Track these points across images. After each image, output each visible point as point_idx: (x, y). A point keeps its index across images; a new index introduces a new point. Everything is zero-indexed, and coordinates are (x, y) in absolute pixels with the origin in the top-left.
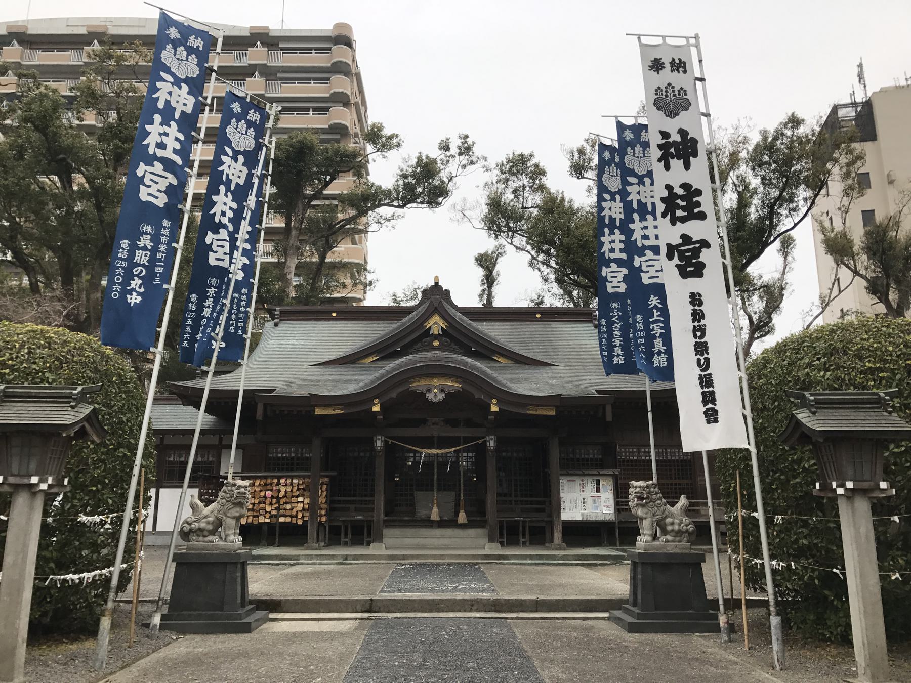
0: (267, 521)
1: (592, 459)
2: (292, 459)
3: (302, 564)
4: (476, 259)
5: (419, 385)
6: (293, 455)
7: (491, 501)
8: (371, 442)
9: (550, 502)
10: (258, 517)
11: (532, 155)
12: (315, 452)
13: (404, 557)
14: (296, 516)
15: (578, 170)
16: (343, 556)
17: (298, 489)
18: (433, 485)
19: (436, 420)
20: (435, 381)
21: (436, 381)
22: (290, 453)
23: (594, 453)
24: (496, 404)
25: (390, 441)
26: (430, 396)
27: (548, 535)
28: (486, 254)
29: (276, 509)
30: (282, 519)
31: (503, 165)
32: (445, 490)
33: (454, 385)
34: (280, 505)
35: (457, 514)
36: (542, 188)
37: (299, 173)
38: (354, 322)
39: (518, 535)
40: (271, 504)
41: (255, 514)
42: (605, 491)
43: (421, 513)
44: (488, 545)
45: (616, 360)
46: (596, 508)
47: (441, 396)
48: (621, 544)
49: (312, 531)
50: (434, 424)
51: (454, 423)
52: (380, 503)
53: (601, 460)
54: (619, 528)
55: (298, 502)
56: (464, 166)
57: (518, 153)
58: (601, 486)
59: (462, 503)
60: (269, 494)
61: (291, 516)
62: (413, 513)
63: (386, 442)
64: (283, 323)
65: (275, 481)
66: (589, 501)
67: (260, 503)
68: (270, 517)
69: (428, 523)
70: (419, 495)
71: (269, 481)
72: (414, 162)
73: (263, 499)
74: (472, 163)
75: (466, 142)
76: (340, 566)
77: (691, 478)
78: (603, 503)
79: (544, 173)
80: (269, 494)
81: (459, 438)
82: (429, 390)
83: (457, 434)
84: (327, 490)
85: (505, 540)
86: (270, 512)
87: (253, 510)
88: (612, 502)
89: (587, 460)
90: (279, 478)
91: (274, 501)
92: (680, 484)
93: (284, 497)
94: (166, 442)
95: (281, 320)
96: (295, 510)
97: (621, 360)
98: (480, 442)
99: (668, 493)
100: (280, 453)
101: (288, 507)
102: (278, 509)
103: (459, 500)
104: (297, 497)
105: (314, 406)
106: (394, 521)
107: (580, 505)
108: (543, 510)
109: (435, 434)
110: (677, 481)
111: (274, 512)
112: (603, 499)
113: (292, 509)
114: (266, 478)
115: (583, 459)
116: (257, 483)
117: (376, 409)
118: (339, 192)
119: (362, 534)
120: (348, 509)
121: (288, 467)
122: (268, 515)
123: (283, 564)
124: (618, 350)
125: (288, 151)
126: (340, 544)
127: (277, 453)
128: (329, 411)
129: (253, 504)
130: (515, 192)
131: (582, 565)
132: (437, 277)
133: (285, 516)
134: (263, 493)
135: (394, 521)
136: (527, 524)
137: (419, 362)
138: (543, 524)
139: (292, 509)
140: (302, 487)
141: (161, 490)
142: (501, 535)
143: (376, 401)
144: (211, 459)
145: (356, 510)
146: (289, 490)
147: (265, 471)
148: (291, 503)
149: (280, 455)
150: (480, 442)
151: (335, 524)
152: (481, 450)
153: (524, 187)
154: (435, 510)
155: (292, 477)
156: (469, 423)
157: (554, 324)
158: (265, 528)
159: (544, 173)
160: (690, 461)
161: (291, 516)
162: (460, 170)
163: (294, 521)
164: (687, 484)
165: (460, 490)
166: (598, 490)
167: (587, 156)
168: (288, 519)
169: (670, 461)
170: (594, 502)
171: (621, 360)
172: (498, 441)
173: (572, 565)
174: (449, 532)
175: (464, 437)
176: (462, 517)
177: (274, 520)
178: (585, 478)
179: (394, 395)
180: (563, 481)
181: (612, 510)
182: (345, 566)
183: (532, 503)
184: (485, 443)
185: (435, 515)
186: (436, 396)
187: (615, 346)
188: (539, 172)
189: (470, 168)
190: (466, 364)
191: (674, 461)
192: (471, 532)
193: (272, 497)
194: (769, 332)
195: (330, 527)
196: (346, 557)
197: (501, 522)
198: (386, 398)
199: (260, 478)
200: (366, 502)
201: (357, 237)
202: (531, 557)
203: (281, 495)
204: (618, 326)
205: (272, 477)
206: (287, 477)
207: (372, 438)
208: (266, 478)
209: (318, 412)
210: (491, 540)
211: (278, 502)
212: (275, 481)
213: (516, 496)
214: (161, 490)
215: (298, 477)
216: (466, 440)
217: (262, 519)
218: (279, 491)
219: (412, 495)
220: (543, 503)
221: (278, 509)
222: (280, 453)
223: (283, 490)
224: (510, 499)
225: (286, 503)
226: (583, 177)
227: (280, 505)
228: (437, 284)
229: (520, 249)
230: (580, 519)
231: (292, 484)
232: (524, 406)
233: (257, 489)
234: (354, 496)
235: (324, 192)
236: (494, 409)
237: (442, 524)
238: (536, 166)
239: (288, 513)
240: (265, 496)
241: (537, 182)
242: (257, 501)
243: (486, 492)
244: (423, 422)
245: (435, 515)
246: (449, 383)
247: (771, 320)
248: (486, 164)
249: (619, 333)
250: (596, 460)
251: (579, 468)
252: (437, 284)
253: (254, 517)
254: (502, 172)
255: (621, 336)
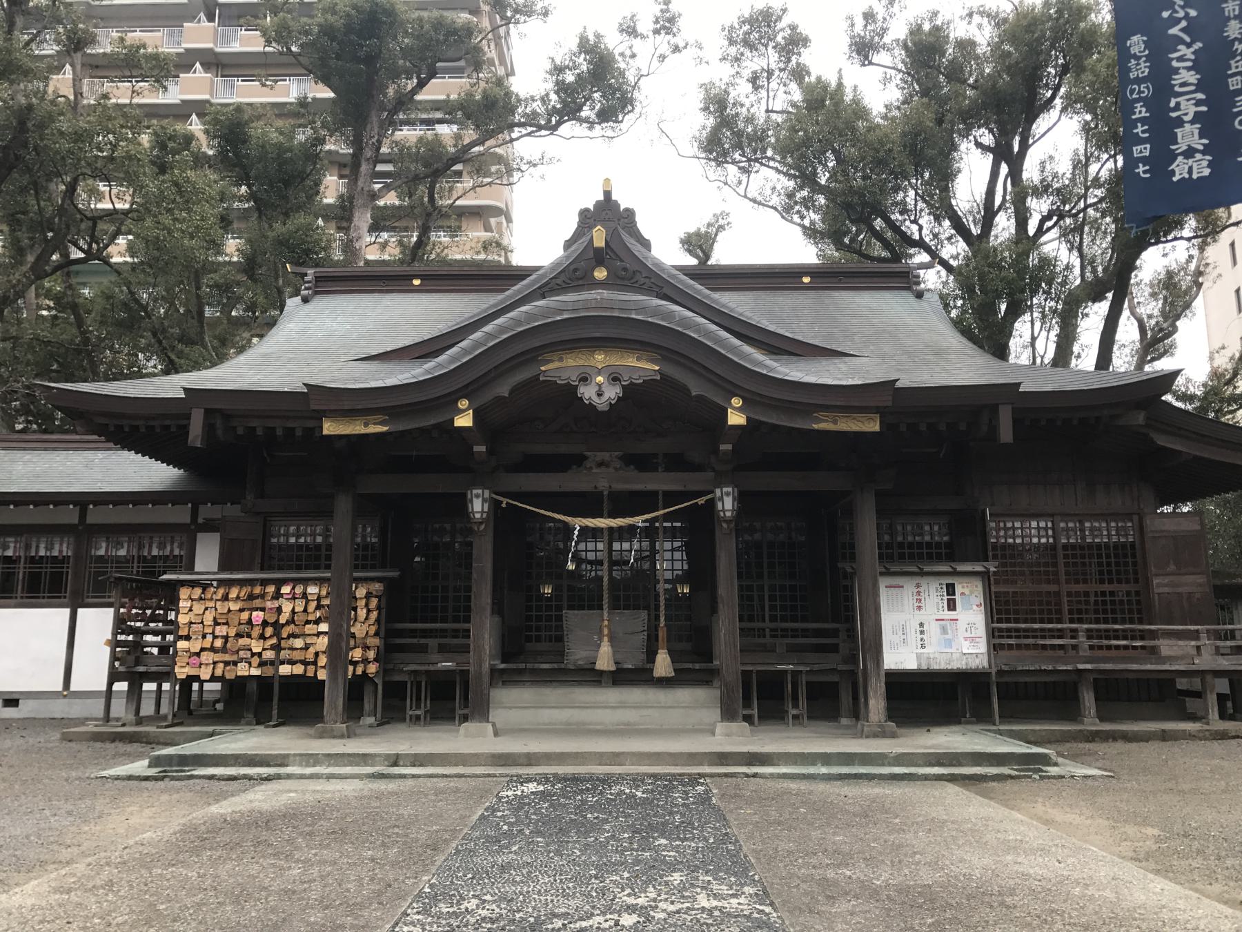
0: (255, 672)
1: (929, 545)
2: (318, 547)
3: (289, 777)
4: (683, 242)
5: (561, 368)
6: (319, 539)
7: (726, 630)
8: (461, 503)
9: (852, 632)
10: (235, 663)
11: (784, 11)
12: (343, 529)
13: (530, 759)
14: (315, 663)
15: (863, 49)
16: (387, 757)
17: (318, 607)
18: (601, 598)
19: (606, 456)
20: (600, 357)
21: (600, 359)
22: (314, 535)
23: (934, 532)
24: (740, 409)
25: (505, 501)
26: (587, 393)
27: (845, 699)
28: (698, 234)
29: (272, 648)
30: (285, 670)
31: (732, 27)
32: (627, 607)
33: (641, 366)
34: (280, 639)
35: (651, 656)
36: (799, 74)
37: (370, 60)
38: (453, 295)
39: (782, 698)
40: (262, 637)
41: (227, 657)
42: (967, 607)
43: (577, 654)
44: (721, 727)
45: (1180, 169)
46: (949, 643)
47: (612, 393)
48: (1007, 716)
49: (334, 699)
50: (601, 464)
51: (642, 463)
52: (485, 634)
53: (948, 545)
54: (998, 684)
55: (319, 634)
56: (663, 58)
57: (760, 6)
58: (957, 597)
59: (662, 634)
60: (258, 616)
61: (305, 663)
62: (561, 654)
63: (495, 505)
64: (318, 297)
65: (271, 589)
66: (933, 629)
67: (239, 635)
68: (262, 664)
69: (590, 676)
70: (572, 618)
71: (257, 590)
72: (573, 44)
73: (245, 628)
74: (676, 49)
75: (667, 11)
76: (381, 785)
77: (1136, 581)
78: (962, 633)
79: (805, 41)
80: (258, 616)
81: (654, 494)
82: (584, 379)
83: (651, 487)
84: (378, 608)
85: (755, 712)
86: (260, 654)
87: (224, 649)
88: (980, 630)
89: (920, 545)
90: (280, 583)
91: (269, 631)
92: (1112, 593)
93: (288, 623)
94: (90, 520)
95: (316, 293)
96: (312, 650)
97: (1201, 168)
98: (701, 501)
99: (1080, 612)
100: (291, 534)
101: (299, 643)
102: (277, 648)
103: (657, 628)
104: (317, 622)
105: (319, 416)
106: (520, 672)
107: (913, 637)
108: (834, 649)
109: (603, 485)
110: (1107, 587)
111: (269, 655)
112: (962, 625)
113: (307, 647)
114: (251, 582)
115: (911, 545)
116: (234, 593)
117: (464, 421)
118: (443, 97)
119: (450, 700)
120: (423, 649)
121: (309, 560)
122: (255, 661)
123: (245, 777)
124: (1189, 136)
125: (348, 15)
126: (404, 720)
127: (287, 535)
128: (356, 428)
129: (226, 638)
130: (754, 80)
131: (952, 779)
132: (607, 180)
133: (292, 662)
134: (245, 616)
135: (520, 672)
136: (804, 679)
137: (561, 311)
138: (835, 678)
139: (307, 647)
140: (326, 602)
141: (80, 611)
142: (747, 703)
143: (463, 404)
144: (176, 552)
145: (443, 649)
146: (299, 609)
147: (262, 569)
148: (304, 635)
149: (292, 540)
150: (701, 501)
151: (397, 678)
152: (698, 528)
153: (770, 73)
154: (606, 648)
155: (306, 582)
156: (677, 463)
157: (837, 295)
158: (253, 687)
159: (805, 41)
160: (1133, 545)
161: (305, 663)
162: (655, 62)
163: (310, 674)
164: (1128, 594)
165: (657, 607)
166: (952, 606)
167: (879, 24)
168: (299, 669)
169: (1090, 546)
170: (944, 630)
171: (1201, 168)
172: (743, 498)
173: (926, 778)
174: (635, 694)
175: (666, 493)
176: (663, 664)
177: (269, 671)
178: (924, 581)
179: (503, 389)
180: (883, 582)
181: (982, 647)
182: (392, 786)
183: (805, 633)
184: (711, 504)
185: (605, 660)
186: (600, 391)
187: (1180, 122)
188: (797, 41)
189: (673, 59)
190: (669, 315)
191: (1099, 546)
192: (684, 695)
193: (265, 623)
194: (1165, 352)
195: (385, 684)
196: (395, 761)
197: (746, 675)
198: (487, 396)
199: (241, 583)
200: (455, 633)
201: (493, 221)
202: (826, 759)
203: (283, 620)
204: (1188, 53)
205: (264, 583)
206: (296, 581)
207: (465, 495)
208: (251, 582)
209: (329, 428)
210: (728, 714)
211: (277, 634)
212: (271, 589)
213: (1058, 594)
214: (80, 611)
215: (319, 581)
216: (671, 497)
217: (243, 670)
218: (279, 610)
219: (559, 618)
220: (835, 633)
221: (277, 648)
222: (291, 534)
223: (287, 607)
224: (761, 625)
225: (293, 636)
226: (871, 63)
227: (280, 639)
228: (607, 194)
229: (759, 203)
230: (915, 667)
231: (305, 595)
232: (808, 410)
233: (234, 607)
234: (444, 621)
235: (418, 97)
236: (736, 419)
237: (621, 677)
238: (793, 28)
239: (297, 656)
240: (250, 622)
241: (794, 59)
242: (232, 633)
243: (714, 610)
244: (574, 461)
245: (605, 660)
246: (631, 361)
247: (1175, 330)
248: (701, 54)
249: (1192, 77)
250: (938, 545)
251: (910, 558)
252: (607, 194)
253: (227, 663)
254: (732, 42)
255: (1199, 87)
